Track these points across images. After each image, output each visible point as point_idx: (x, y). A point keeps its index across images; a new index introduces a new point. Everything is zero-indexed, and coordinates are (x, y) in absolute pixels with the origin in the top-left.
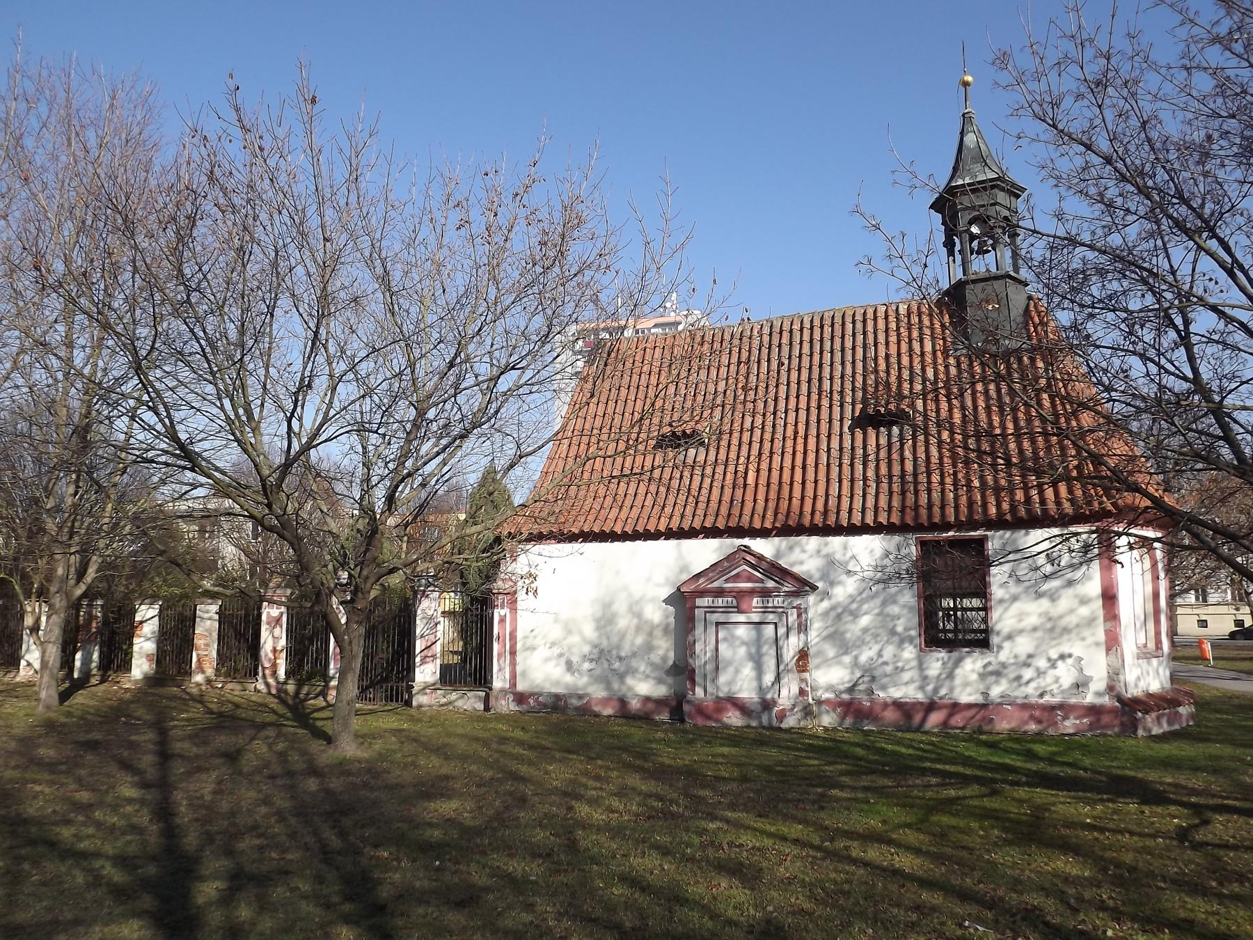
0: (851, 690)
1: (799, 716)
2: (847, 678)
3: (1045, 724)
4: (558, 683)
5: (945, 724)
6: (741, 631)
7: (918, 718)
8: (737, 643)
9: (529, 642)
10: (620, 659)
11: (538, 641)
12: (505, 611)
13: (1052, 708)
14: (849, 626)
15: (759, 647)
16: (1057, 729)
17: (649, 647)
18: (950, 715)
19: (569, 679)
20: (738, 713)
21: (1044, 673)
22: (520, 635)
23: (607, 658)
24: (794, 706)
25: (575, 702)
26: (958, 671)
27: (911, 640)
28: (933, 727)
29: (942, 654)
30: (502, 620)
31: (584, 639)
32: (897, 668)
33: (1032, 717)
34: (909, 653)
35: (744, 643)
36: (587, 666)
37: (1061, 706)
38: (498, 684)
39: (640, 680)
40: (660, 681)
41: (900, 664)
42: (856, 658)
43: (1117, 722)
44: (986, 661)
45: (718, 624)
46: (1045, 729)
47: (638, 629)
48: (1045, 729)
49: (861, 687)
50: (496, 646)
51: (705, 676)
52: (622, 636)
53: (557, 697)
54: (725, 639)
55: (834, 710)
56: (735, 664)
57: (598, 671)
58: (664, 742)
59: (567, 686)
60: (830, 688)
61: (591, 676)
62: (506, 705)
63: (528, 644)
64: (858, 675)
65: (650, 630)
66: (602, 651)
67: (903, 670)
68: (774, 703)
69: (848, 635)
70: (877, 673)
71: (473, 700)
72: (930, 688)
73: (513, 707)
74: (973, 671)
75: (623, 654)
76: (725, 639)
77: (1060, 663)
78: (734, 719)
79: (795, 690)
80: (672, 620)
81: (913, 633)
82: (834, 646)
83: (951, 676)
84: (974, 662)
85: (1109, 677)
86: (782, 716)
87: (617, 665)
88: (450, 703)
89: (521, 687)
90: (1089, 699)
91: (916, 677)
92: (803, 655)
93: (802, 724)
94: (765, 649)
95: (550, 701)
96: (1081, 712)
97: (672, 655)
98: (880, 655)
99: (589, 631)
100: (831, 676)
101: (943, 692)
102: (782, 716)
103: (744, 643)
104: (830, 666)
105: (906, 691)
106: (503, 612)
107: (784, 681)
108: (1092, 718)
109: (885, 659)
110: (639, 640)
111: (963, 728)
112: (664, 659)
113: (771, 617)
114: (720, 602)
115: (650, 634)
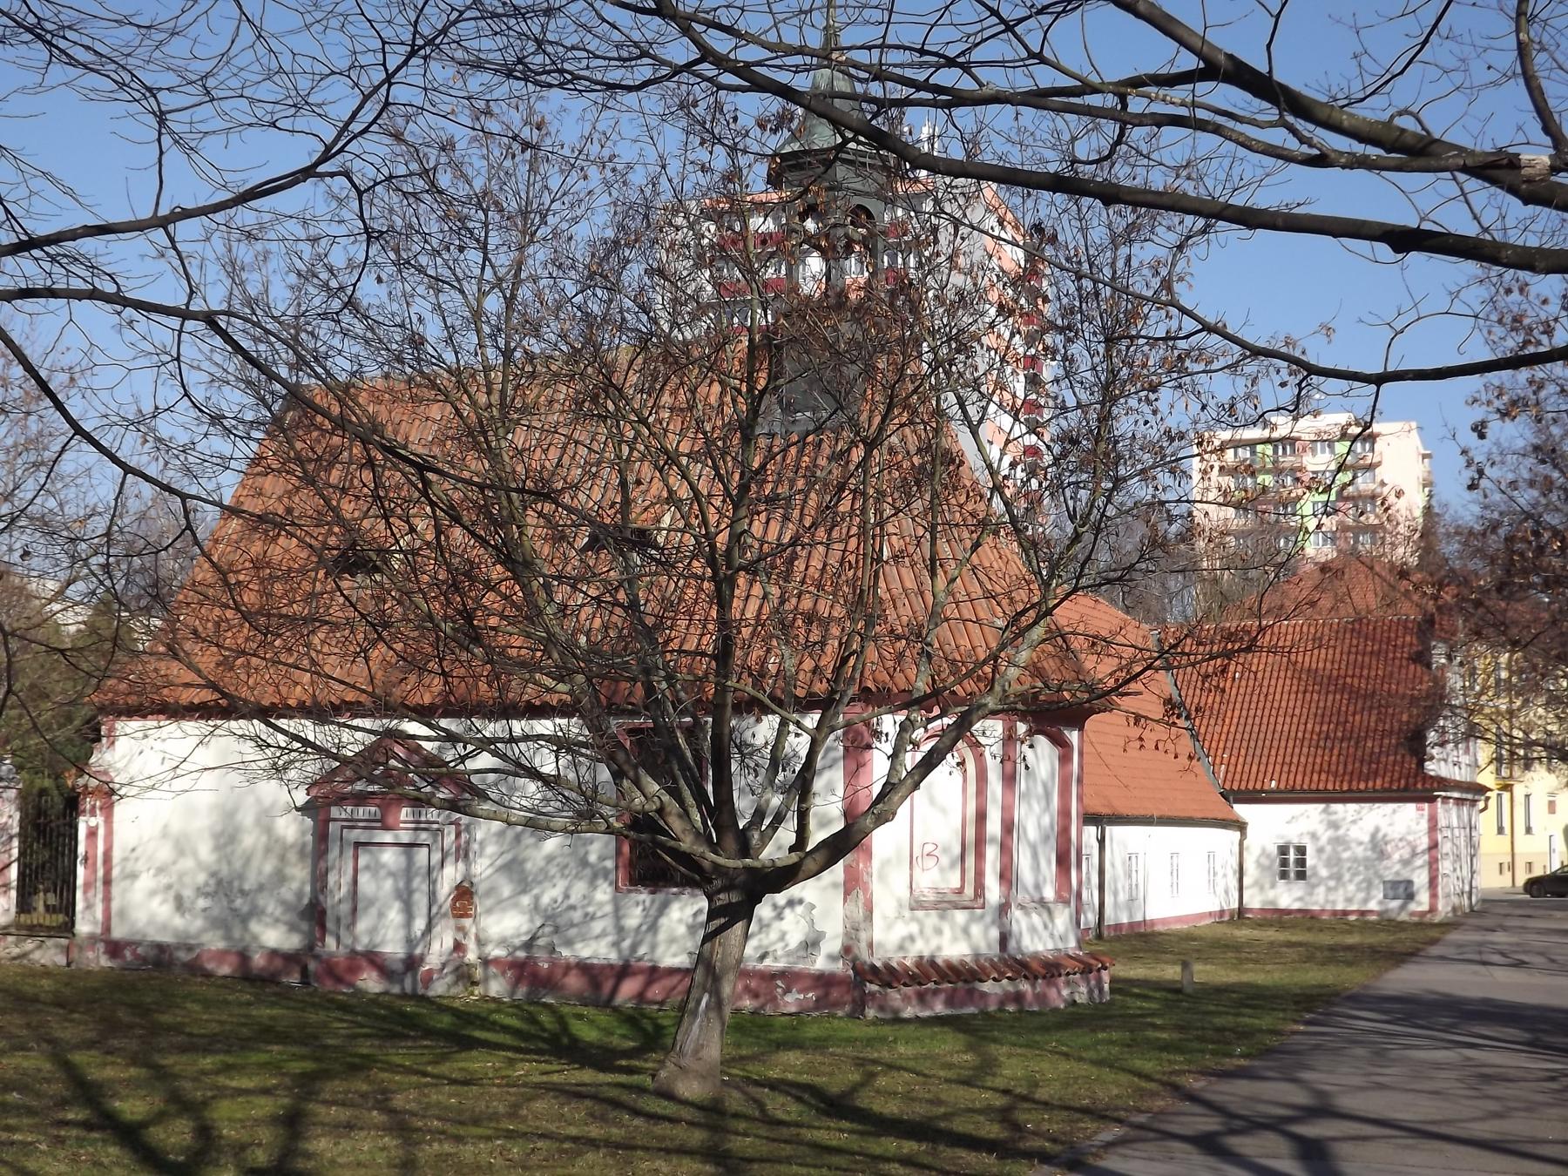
0: (529, 945)
1: (449, 979)
2: (525, 928)
3: (762, 1000)
4: (164, 927)
5: (640, 996)
6: (389, 857)
7: (608, 986)
8: (383, 873)
9: (130, 866)
10: (243, 893)
11: (140, 866)
12: (97, 820)
13: (771, 977)
14: (528, 853)
15: (409, 881)
16: (777, 1006)
17: (280, 877)
18: (649, 984)
19: (178, 922)
20: (374, 974)
21: (768, 926)
22: (117, 855)
23: (228, 893)
24: (444, 965)
25: (183, 956)
26: (664, 921)
27: (605, 874)
28: (626, 1002)
29: (644, 896)
30: (92, 833)
31: (201, 865)
32: (586, 915)
33: (747, 989)
34: (603, 893)
35: (392, 874)
36: (202, 903)
37: (783, 974)
38: (83, 927)
39: (267, 925)
40: (292, 928)
41: (590, 910)
42: (537, 898)
43: (848, 998)
44: (696, 908)
45: (358, 845)
46: (762, 1007)
47: (268, 850)
48: (762, 1007)
49: (541, 942)
50: (80, 870)
51: (338, 920)
52: (248, 861)
53: (161, 948)
54: (367, 868)
55: (504, 973)
56: (377, 905)
57: (216, 912)
58: (311, 1015)
59: (176, 933)
60: (503, 942)
61: (206, 918)
62: (99, 960)
63: (128, 870)
64: (538, 924)
65: (276, 847)
66: (219, 883)
67: (593, 918)
68: (422, 959)
69: (529, 866)
70: (561, 921)
71: (53, 951)
72: (626, 944)
73: (105, 962)
74: (680, 921)
75: (247, 887)
76: (367, 868)
77: (787, 912)
78: (371, 982)
79: (449, 943)
80: (309, 838)
81: (610, 864)
82: (511, 880)
83: (653, 927)
84: (681, 909)
85: (846, 934)
86: (428, 979)
87: (238, 902)
88: (24, 955)
89: (118, 933)
90: (820, 964)
91: (610, 929)
92: (464, 893)
93: (453, 991)
94: (416, 882)
95: (152, 953)
96: (808, 983)
97: (308, 888)
98: (567, 896)
99: (205, 851)
100: (504, 925)
101: (642, 951)
102: (428, 979)
103: (392, 874)
104: (504, 910)
105: (597, 949)
106: (93, 822)
107: (437, 930)
108: (820, 992)
109: (572, 901)
110: (268, 868)
111: (662, 1003)
112: (300, 895)
113: (424, 837)
114: (361, 812)
115: (282, 858)
